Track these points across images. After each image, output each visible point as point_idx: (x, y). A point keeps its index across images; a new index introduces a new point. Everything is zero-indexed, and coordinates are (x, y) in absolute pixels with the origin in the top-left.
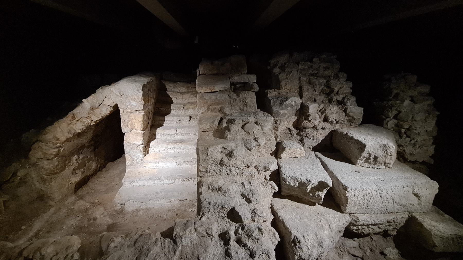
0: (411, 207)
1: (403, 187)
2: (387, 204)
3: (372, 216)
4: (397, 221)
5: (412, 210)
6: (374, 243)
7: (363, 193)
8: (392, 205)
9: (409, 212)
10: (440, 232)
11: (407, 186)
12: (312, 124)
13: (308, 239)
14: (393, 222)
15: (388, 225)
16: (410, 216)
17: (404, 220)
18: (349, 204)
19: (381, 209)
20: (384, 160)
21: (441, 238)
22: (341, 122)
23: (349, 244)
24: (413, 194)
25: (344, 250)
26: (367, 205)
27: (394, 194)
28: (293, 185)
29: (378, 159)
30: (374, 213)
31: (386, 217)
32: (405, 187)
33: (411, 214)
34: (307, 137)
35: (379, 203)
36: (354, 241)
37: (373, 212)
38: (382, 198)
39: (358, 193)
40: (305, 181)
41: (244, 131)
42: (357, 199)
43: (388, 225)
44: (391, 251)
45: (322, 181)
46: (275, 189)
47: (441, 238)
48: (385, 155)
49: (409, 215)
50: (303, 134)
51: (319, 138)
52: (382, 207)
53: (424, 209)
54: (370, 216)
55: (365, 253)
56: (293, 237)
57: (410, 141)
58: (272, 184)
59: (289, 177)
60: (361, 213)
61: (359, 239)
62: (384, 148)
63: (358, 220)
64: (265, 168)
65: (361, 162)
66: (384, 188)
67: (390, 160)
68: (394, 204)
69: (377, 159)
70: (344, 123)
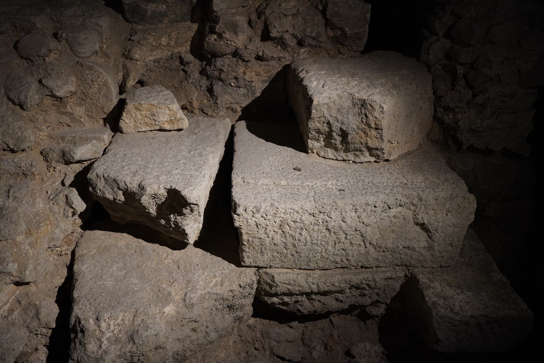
0: (408, 254)
1: (387, 206)
2: (347, 245)
3: (311, 275)
4: (376, 285)
5: (412, 261)
6: (335, 333)
7: (278, 220)
8: (360, 248)
9: (406, 266)
10: (452, 310)
11: (401, 206)
12: (228, 43)
13: (109, 325)
14: (367, 288)
15: (360, 295)
16: (409, 276)
17: (397, 286)
18: (248, 245)
19: (332, 259)
20: (363, 141)
21: (450, 323)
22: (311, 41)
23: (277, 334)
24: (417, 224)
25: (263, 347)
26: (295, 249)
27: (363, 223)
28: (111, 197)
29: (350, 137)
30: (316, 267)
31: (347, 277)
32: (391, 207)
33: (410, 272)
34: (222, 80)
35: (326, 245)
36: (291, 327)
37: (312, 265)
38: (333, 234)
39: (264, 221)
40: (133, 187)
41: (19, 55)
42: (266, 233)
43: (360, 295)
44: (367, 350)
45: (174, 189)
46: (73, 208)
47: (450, 323)
48: (364, 126)
49: (407, 273)
50: (211, 71)
51: (253, 84)
52: (334, 254)
53: (440, 260)
54: (307, 274)
55: (310, 352)
56: (74, 319)
57: (474, 96)
58: (68, 195)
59: (102, 176)
60: (282, 267)
61: (304, 323)
62: (361, 110)
63: (274, 282)
64: (64, 154)
65: (317, 145)
66: (334, 207)
67: (380, 140)
68: (366, 247)
69: (348, 136)
70: (320, 47)
